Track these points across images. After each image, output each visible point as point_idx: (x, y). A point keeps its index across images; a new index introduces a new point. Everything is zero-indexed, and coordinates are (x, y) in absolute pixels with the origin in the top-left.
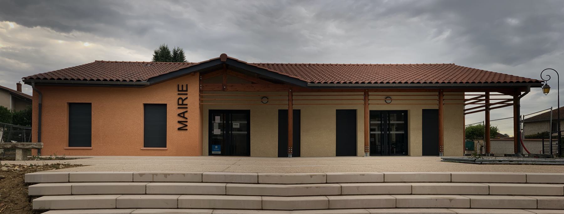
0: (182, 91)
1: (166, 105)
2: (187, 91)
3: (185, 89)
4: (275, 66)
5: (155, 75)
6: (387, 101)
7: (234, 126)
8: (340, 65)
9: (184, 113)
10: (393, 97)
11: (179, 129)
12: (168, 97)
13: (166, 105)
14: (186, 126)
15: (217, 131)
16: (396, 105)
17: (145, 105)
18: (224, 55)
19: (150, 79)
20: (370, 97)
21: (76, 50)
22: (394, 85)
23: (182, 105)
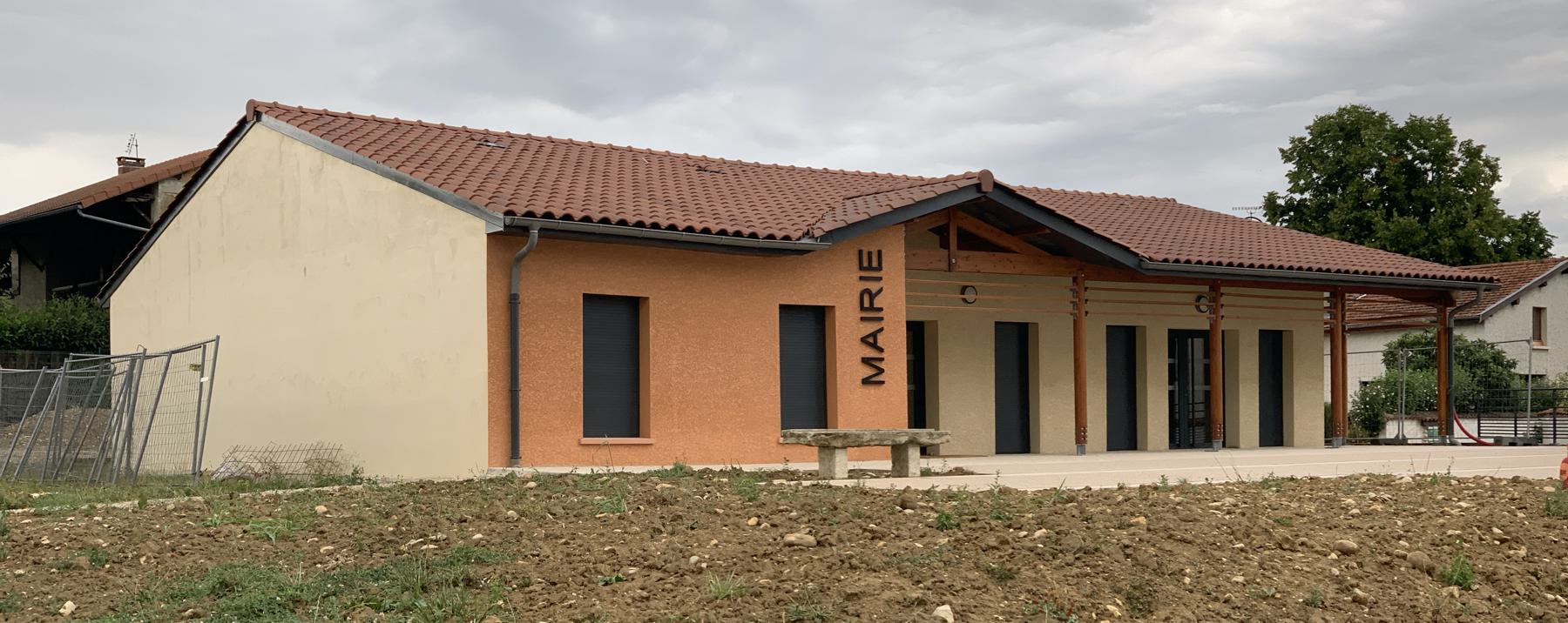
0: (870, 268)
2: (879, 268)
3: (875, 264)
9: (874, 335)
11: (866, 381)
12: (833, 287)
14: (881, 371)
17: (784, 309)
20: (1223, 300)
23: (869, 306)
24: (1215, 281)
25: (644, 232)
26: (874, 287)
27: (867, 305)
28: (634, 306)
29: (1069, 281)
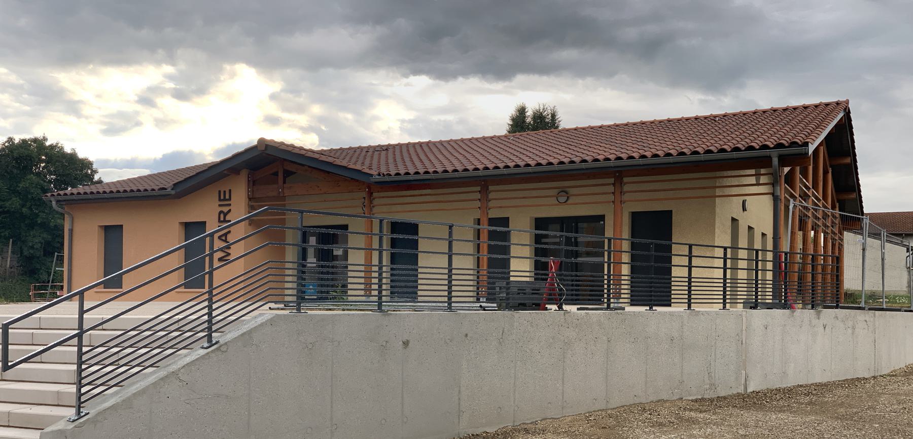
0: (225, 200)
1: (121, 226)
2: (230, 199)
3: (227, 197)
4: (418, 147)
5: (181, 179)
6: (560, 199)
7: (335, 253)
8: (584, 129)
9: (226, 235)
10: (572, 191)
12: (205, 210)
13: (121, 226)
14: (229, 254)
15: (312, 260)
16: (578, 207)
18: (261, 141)
19: (175, 185)
21: (591, 101)
22: (709, 157)
24: (620, 172)
25: (123, 195)
26: (225, 209)
27: (222, 219)
28: (413, 228)
29: (364, 194)
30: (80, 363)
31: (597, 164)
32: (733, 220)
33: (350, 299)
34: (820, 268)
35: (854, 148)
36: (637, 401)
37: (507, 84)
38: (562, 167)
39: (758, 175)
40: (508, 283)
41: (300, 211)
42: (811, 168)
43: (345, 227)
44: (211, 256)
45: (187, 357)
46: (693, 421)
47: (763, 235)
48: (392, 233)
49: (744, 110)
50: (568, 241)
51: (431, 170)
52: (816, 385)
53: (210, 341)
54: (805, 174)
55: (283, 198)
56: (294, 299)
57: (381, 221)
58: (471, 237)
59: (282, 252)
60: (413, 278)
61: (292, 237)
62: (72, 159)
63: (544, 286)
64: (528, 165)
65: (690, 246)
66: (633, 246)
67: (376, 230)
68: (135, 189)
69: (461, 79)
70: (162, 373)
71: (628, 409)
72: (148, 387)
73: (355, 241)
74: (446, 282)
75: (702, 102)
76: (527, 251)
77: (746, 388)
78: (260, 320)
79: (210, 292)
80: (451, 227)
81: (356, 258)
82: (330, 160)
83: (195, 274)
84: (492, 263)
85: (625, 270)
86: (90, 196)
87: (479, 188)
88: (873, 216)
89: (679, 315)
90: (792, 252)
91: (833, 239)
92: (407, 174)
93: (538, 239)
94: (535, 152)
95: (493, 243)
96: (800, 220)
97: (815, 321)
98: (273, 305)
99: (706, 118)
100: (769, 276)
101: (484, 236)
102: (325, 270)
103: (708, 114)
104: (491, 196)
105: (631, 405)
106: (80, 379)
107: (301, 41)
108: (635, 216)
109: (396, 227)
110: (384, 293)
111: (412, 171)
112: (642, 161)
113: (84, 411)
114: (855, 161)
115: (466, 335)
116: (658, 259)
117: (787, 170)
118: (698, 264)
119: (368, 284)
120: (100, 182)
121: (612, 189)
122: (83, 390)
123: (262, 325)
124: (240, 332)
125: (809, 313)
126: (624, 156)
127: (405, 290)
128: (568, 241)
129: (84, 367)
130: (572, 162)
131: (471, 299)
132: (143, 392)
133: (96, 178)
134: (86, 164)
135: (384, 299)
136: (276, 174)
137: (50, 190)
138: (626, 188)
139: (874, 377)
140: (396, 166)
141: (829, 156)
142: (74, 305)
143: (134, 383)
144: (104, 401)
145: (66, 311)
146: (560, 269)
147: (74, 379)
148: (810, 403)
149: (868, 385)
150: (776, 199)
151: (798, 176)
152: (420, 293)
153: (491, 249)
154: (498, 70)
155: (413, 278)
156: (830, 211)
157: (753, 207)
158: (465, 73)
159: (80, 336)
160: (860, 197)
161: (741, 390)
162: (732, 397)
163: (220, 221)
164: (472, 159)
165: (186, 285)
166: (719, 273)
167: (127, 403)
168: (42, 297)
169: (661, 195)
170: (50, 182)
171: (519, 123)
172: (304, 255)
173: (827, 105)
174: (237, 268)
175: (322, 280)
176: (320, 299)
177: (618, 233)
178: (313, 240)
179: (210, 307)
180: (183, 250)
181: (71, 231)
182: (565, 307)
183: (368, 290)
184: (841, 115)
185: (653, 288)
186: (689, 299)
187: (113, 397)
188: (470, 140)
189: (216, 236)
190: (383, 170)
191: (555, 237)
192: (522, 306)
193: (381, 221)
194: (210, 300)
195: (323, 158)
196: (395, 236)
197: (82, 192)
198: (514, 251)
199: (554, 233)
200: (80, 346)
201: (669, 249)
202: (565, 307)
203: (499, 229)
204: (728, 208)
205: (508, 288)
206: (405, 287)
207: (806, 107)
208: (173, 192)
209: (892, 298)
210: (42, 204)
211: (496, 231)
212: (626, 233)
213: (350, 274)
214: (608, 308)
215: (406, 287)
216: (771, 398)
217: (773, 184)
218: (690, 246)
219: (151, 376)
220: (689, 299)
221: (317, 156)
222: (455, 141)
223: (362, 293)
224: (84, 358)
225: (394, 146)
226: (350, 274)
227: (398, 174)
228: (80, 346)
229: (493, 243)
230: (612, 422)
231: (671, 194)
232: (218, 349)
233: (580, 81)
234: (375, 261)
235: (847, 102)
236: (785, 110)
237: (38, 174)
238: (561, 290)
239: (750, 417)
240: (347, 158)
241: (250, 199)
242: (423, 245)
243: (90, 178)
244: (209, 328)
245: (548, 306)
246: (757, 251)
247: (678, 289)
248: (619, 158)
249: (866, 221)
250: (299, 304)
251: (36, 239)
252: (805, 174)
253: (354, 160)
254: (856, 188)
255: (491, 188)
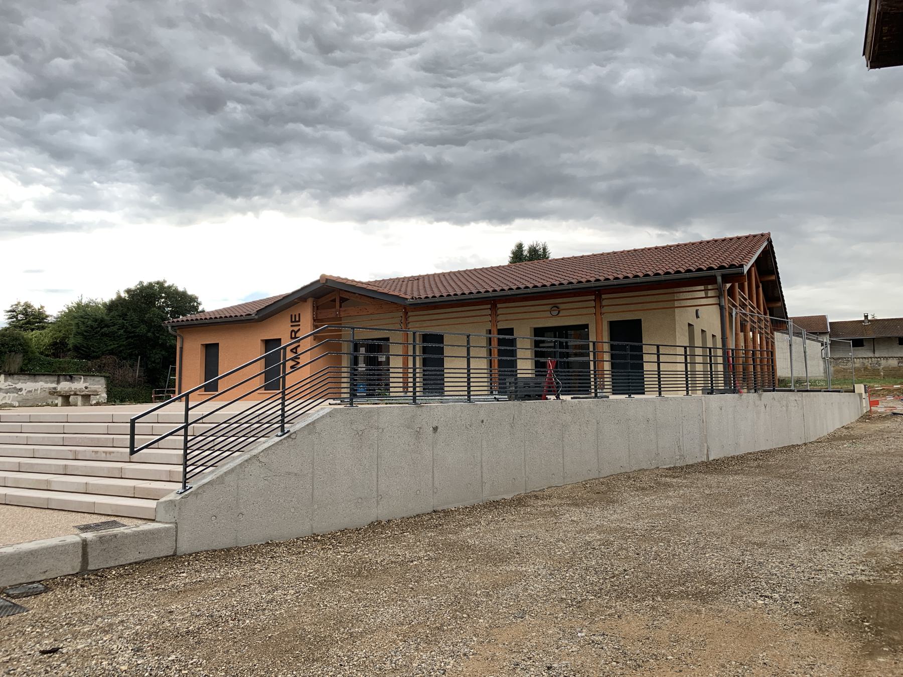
0: (295, 321)
4: (442, 277)
9: (296, 348)
10: (562, 306)
12: (280, 330)
15: (362, 367)
21: (574, 237)
22: (668, 277)
24: (599, 291)
26: (296, 329)
28: (439, 338)
29: (401, 314)
30: (186, 448)
31: (580, 285)
32: (690, 325)
33: (392, 394)
34: (758, 360)
35: (777, 268)
36: (623, 471)
37: (507, 226)
38: (553, 288)
39: (706, 290)
40: (516, 379)
41: (356, 333)
42: (746, 284)
43: (387, 339)
44: (284, 364)
45: (265, 443)
46: (668, 485)
47: (713, 336)
48: (424, 342)
49: (693, 241)
50: (561, 345)
51: (452, 294)
52: (762, 452)
53: (283, 430)
54: (742, 288)
55: (340, 319)
56: (348, 395)
57: (414, 333)
58: (484, 343)
59: (339, 359)
60: (440, 377)
61: (347, 348)
62: (184, 295)
63: (544, 381)
64: (527, 287)
65: (658, 346)
66: (612, 347)
67: (411, 341)
68: (228, 315)
69: (473, 224)
70: (246, 456)
71: (617, 477)
72: (235, 467)
73: (395, 349)
74: (466, 380)
75: (659, 236)
76: (529, 354)
77: (708, 457)
78: (321, 413)
79: (283, 392)
80: (468, 337)
81: (396, 363)
82: (375, 288)
83: (273, 379)
84: (501, 364)
85: (607, 366)
86: (195, 322)
87: (489, 306)
88: (797, 320)
89: (652, 401)
90: (737, 349)
91: (767, 338)
92: (434, 297)
93: (537, 344)
94: (532, 278)
95: (503, 348)
96: (741, 324)
97: (758, 402)
98: (332, 401)
99: (663, 247)
100: (720, 368)
101: (495, 343)
102: (371, 373)
103: (665, 245)
104: (499, 312)
105: (618, 475)
106: (186, 460)
107: (353, 201)
108: (612, 324)
109: (426, 338)
110: (418, 389)
111: (438, 295)
112: (616, 282)
113: (188, 485)
114: (779, 278)
115: (482, 421)
116: (633, 357)
117: (728, 285)
118: (663, 359)
119: (405, 383)
120: (203, 311)
121: (593, 303)
122: (188, 469)
123: (323, 417)
124: (307, 423)
125: (753, 396)
126: (602, 278)
127: (434, 387)
128: (561, 345)
129: (188, 451)
130: (561, 284)
131: (486, 393)
132: (232, 470)
133: (200, 309)
134: (193, 299)
135: (418, 394)
136: (334, 301)
137: (168, 319)
138: (604, 303)
139: (805, 444)
140: (425, 291)
141: (759, 275)
142: (183, 404)
143: (225, 464)
144: (204, 478)
145: (175, 409)
146: (556, 367)
147: (181, 461)
148: (758, 466)
149: (800, 450)
150: (722, 308)
151: (737, 290)
152: (446, 389)
153: (501, 353)
154: (503, 217)
155: (440, 377)
156: (762, 317)
157: (704, 315)
158: (476, 220)
159: (185, 428)
160: (784, 305)
161: (704, 459)
162: (698, 464)
163: (292, 338)
164: (483, 284)
165: (267, 388)
166: (681, 367)
167: (221, 479)
168: (160, 399)
169: (632, 307)
170: (167, 313)
171: (518, 255)
172: (355, 361)
173: (754, 236)
174: (304, 373)
175: (369, 380)
176: (369, 395)
177: (600, 337)
178: (362, 350)
179: (283, 404)
180: (263, 360)
181: (181, 348)
182: (561, 397)
183: (405, 388)
184: (765, 244)
185: (629, 379)
186: (660, 388)
187: (210, 475)
188: (481, 269)
189: (288, 349)
190: (416, 295)
191: (551, 342)
192: (528, 397)
193: (414, 333)
194: (283, 398)
195: (370, 287)
196: (426, 356)
197: (189, 319)
198: (520, 354)
199: (549, 339)
200: (186, 435)
201: (640, 349)
202: (561, 397)
203: (507, 337)
204: (684, 317)
205: (516, 383)
206: (434, 384)
207: (739, 238)
208: (256, 317)
209: (814, 382)
210: (161, 329)
211: (504, 339)
212: (606, 337)
213: (391, 375)
214: (596, 396)
215: (434, 384)
216: (728, 464)
217: (719, 296)
218: (658, 346)
219: (238, 458)
220: (660, 388)
221: (365, 286)
222: (470, 271)
223: (401, 390)
224: (189, 445)
225: (423, 277)
226: (391, 375)
227: (427, 297)
228: (186, 435)
229: (503, 348)
230: (604, 488)
231: (639, 307)
232: (288, 437)
233: (564, 223)
234: (411, 365)
235: (769, 234)
236: (724, 240)
237: (159, 307)
238: (558, 383)
239: (713, 479)
240: (388, 287)
241: (314, 320)
242: (447, 351)
243: (195, 309)
244: (282, 421)
245: (548, 397)
246: (710, 349)
247: (650, 380)
248: (598, 280)
249: (791, 323)
250: (351, 400)
251: (157, 355)
252: (742, 288)
253: (393, 288)
254: (780, 298)
255: (499, 306)
